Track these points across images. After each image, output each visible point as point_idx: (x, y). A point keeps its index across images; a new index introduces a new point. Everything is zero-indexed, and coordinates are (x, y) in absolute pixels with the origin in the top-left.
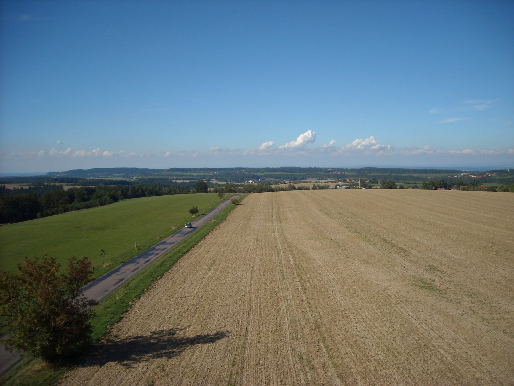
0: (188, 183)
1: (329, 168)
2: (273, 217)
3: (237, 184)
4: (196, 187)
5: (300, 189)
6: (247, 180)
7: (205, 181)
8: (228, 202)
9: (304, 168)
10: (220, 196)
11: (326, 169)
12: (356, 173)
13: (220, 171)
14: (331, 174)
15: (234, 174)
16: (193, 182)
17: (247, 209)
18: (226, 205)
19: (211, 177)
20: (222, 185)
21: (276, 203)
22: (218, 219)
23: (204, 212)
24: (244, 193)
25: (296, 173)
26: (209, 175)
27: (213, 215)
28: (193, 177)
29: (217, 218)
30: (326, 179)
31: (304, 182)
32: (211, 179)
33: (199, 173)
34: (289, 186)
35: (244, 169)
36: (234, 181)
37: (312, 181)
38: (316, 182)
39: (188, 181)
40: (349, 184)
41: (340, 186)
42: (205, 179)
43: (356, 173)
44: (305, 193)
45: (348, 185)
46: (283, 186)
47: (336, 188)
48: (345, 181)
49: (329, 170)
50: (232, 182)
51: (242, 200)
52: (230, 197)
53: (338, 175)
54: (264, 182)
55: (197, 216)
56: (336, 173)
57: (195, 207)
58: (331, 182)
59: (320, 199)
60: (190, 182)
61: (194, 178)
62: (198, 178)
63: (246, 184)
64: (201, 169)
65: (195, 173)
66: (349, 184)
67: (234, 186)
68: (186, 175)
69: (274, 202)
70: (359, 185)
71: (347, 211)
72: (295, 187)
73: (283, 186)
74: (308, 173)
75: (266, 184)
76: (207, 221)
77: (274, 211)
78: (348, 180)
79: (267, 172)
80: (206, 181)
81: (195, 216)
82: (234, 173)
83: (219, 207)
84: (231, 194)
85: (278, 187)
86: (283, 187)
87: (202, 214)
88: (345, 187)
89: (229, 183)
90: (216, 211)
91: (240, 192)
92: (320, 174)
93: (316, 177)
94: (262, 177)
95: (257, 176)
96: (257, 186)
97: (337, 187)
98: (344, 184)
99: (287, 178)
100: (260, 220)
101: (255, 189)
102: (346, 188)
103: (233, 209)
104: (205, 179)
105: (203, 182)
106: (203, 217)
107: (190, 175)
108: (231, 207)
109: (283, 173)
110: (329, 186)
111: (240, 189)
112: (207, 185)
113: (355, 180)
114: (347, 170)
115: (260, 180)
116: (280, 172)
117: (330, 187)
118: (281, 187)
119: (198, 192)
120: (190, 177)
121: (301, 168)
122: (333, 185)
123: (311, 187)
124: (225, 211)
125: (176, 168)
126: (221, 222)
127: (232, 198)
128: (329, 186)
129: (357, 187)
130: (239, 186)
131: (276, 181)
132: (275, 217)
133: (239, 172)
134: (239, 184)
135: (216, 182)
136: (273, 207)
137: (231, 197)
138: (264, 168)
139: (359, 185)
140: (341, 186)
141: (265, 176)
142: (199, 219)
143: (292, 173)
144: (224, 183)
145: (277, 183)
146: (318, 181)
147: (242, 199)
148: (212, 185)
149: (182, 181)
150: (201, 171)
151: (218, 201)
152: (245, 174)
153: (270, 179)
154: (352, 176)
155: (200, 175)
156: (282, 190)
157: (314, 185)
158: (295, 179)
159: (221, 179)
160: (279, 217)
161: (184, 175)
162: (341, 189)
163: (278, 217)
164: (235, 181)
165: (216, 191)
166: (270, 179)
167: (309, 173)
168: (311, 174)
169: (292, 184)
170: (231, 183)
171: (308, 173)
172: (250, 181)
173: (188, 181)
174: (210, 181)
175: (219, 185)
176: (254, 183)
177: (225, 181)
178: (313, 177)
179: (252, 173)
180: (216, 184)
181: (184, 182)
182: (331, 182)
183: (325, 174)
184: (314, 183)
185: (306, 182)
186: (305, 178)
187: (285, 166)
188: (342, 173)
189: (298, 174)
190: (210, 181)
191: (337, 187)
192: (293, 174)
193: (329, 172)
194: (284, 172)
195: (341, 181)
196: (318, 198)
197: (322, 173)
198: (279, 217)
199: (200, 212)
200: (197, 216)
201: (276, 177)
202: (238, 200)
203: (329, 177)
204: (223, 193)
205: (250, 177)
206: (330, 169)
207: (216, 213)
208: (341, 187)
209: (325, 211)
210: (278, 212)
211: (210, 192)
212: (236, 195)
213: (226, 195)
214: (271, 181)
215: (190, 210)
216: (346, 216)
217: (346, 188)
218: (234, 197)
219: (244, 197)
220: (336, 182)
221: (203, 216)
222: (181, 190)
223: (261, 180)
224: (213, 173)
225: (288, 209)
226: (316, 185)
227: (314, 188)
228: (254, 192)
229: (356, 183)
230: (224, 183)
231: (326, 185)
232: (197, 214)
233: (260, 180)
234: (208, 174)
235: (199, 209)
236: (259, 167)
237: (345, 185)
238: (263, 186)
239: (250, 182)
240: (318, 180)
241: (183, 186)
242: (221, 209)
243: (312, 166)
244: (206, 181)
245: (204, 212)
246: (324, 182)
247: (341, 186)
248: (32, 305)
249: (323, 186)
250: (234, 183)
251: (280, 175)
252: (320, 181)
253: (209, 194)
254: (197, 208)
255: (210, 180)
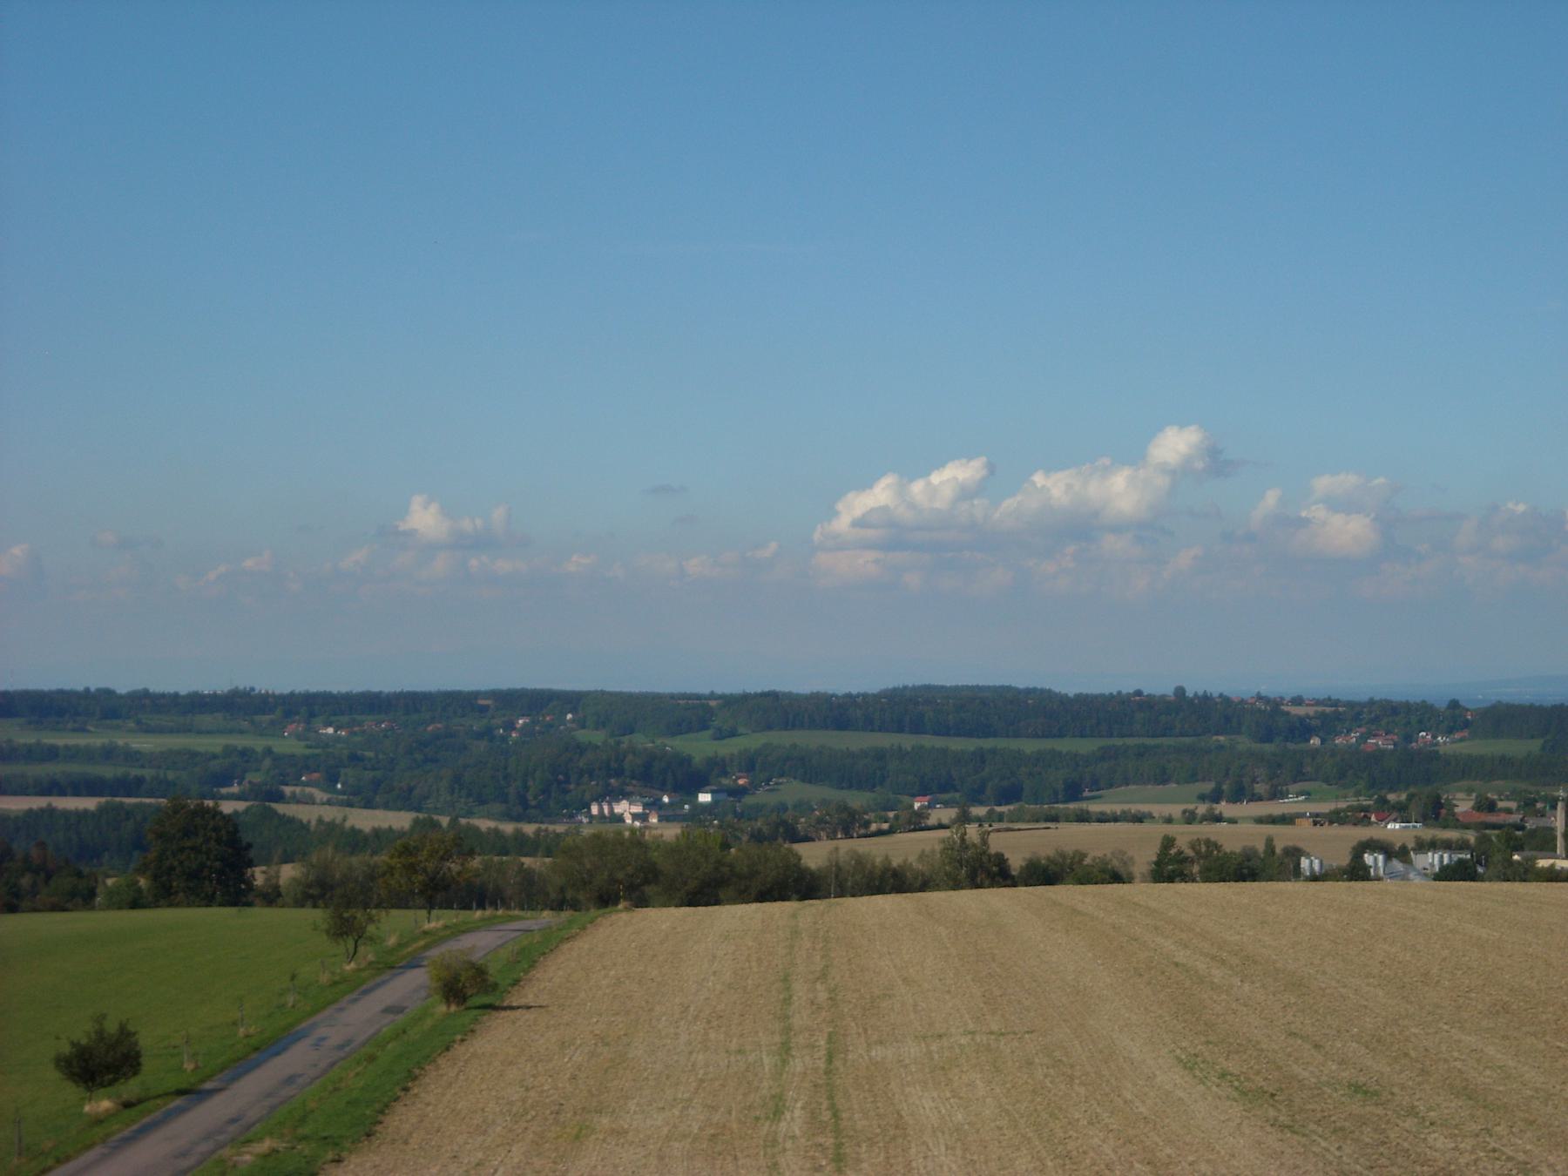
0: (82, 815)
1: (1298, 701)
2: (778, 1113)
3: (508, 828)
4: (152, 855)
5: (1044, 874)
6: (599, 799)
7: (227, 807)
8: (411, 985)
9: (1082, 700)
10: (344, 929)
11: (1275, 704)
12: (1534, 746)
13: (369, 723)
14: (1314, 753)
15: (482, 746)
16: (129, 813)
17: (563, 1045)
18: (388, 1010)
19: (291, 768)
20: (379, 837)
21: (823, 996)
22: (305, 1130)
23: (189, 1066)
24: (559, 905)
25: (1014, 744)
26: (269, 751)
27: (269, 1095)
28: (135, 772)
29: (303, 1120)
30: (1276, 795)
31: (1083, 818)
32: (288, 790)
33: (186, 730)
34: (948, 846)
35: (572, 700)
36: (482, 801)
37: (1157, 809)
38: (1190, 818)
39: (89, 804)
40: (1471, 836)
41: (1389, 851)
42: (235, 789)
43: (1534, 746)
44: (1075, 911)
45: (1462, 846)
46: (905, 849)
47: (1357, 872)
48: (1436, 812)
49: (1301, 719)
50: (469, 814)
51: (533, 964)
52: (435, 939)
53: (1378, 755)
54: (739, 816)
55: (128, 1105)
56: (1363, 738)
57: (111, 1027)
58: (1317, 820)
59: (1201, 966)
60: (102, 810)
61: (140, 781)
62: (171, 775)
63: (587, 831)
64: (198, 704)
65: (149, 730)
66: (1471, 836)
67: (465, 844)
68: (73, 754)
69: (800, 990)
70: (1560, 843)
71: (1424, 1072)
72: (1000, 860)
73: (905, 849)
74: (1118, 742)
75: (758, 837)
76: (204, 1147)
77: (797, 1065)
78: (1463, 806)
79: (769, 727)
80: (241, 806)
81: (106, 1104)
82: (487, 733)
83: (322, 1031)
84: (438, 920)
85: (860, 861)
86: (895, 863)
87: (173, 1082)
88: (1433, 860)
89: (445, 821)
90: (296, 1059)
91: (532, 894)
92: (1221, 747)
93: (1193, 777)
94: (725, 774)
95: (685, 761)
96: (673, 850)
97: (1368, 859)
98: (1428, 833)
99: (938, 786)
100: (668, 1138)
101: (651, 874)
102: (1446, 874)
103: (443, 1042)
104: (235, 789)
105: (215, 813)
106: (181, 1111)
107: (109, 753)
108: (429, 1022)
109: (907, 741)
110: (1295, 853)
111: (528, 877)
112: (246, 837)
113: (1528, 804)
114: (1454, 717)
115: (705, 798)
116: (883, 729)
117: (1305, 863)
118: (878, 860)
119: (164, 895)
120: (108, 772)
121: (1063, 701)
122: (1337, 843)
123: (1144, 857)
124: (372, 1059)
125: (145, 694)
126: (330, 1156)
127: (444, 948)
128: (1295, 853)
129: (1543, 863)
130: (524, 845)
131: (843, 808)
132: (794, 1121)
133: (524, 731)
134: (529, 829)
135: (331, 814)
136: (788, 1030)
137: (443, 940)
138: (745, 697)
139: (1560, 843)
140: (1402, 854)
141: (750, 763)
142: (144, 1131)
143: (988, 743)
144: (400, 820)
145: (849, 824)
146: (1202, 809)
147: (528, 959)
148: (295, 841)
149: (38, 803)
150: (205, 720)
151: (324, 978)
152: (581, 749)
153: (791, 791)
154: (1502, 767)
155: (193, 755)
156: (893, 881)
157: (1168, 842)
158: (1010, 794)
159: (377, 784)
160: (836, 1115)
161: (52, 754)
162: (1404, 877)
163: (826, 1116)
164: (498, 807)
165: (316, 892)
166: (791, 791)
167: (1130, 741)
168: (1142, 753)
169: (972, 831)
170: (454, 821)
171: (1118, 742)
172: (622, 807)
173: (89, 804)
174: (281, 808)
175: (356, 841)
176: (654, 820)
177: (404, 801)
178: (1162, 778)
179: (642, 741)
180: (330, 830)
181: (51, 811)
182: (1317, 820)
183: (1268, 748)
184: (1171, 830)
185: (1102, 818)
186: (1096, 785)
187: (940, 684)
188: (1409, 738)
189: (1029, 746)
190: (281, 808)
191: (1368, 859)
192: (994, 751)
193: (1302, 729)
194: (917, 728)
195: (1401, 812)
196: (1181, 956)
197: (1244, 743)
198: (836, 1115)
199: (152, 1074)
200: (128, 1105)
201: (847, 773)
202: (493, 970)
203: (1299, 776)
204: (366, 906)
205: (619, 773)
206: (1311, 711)
207: (290, 1080)
208: (1397, 865)
209: (1232, 1066)
210: (828, 1072)
211: (272, 897)
212: (487, 924)
213: (393, 925)
214: (803, 807)
215: (66, 1049)
216: (1412, 1111)
217: (1446, 874)
218: (466, 942)
219: (550, 944)
220: (1359, 817)
221: (179, 1102)
222: (26, 881)
223: (715, 803)
224: (299, 737)
225: (912, 1050)
226: (1183, 843)
227: (1170, 868)
228: (642, 902)
229: (1530, 824)
230: (400, 820)
231: (1270, 842)
232: (131, 1088)
233: (705, 798)
234: (258, 744)
235: (146, 1040)
236: (705, 690)
237: (1433, 845)
238: (726, 846)
239: (620, 819)
240: (1202, 798)
241: (42, 845)
242: (341, 1047)
243: (1158, 682)
244: (241, 806)
245: (189, 1066)
246: (1260, 820)
247: (1402, 854)
248: (994, 1157)
249: (1249, 855)
250: (485, 824)
251: (880, 755)
252: (1224, 808)
253: (259, 914)
254: (125, 1033)
255: (280, 798)
